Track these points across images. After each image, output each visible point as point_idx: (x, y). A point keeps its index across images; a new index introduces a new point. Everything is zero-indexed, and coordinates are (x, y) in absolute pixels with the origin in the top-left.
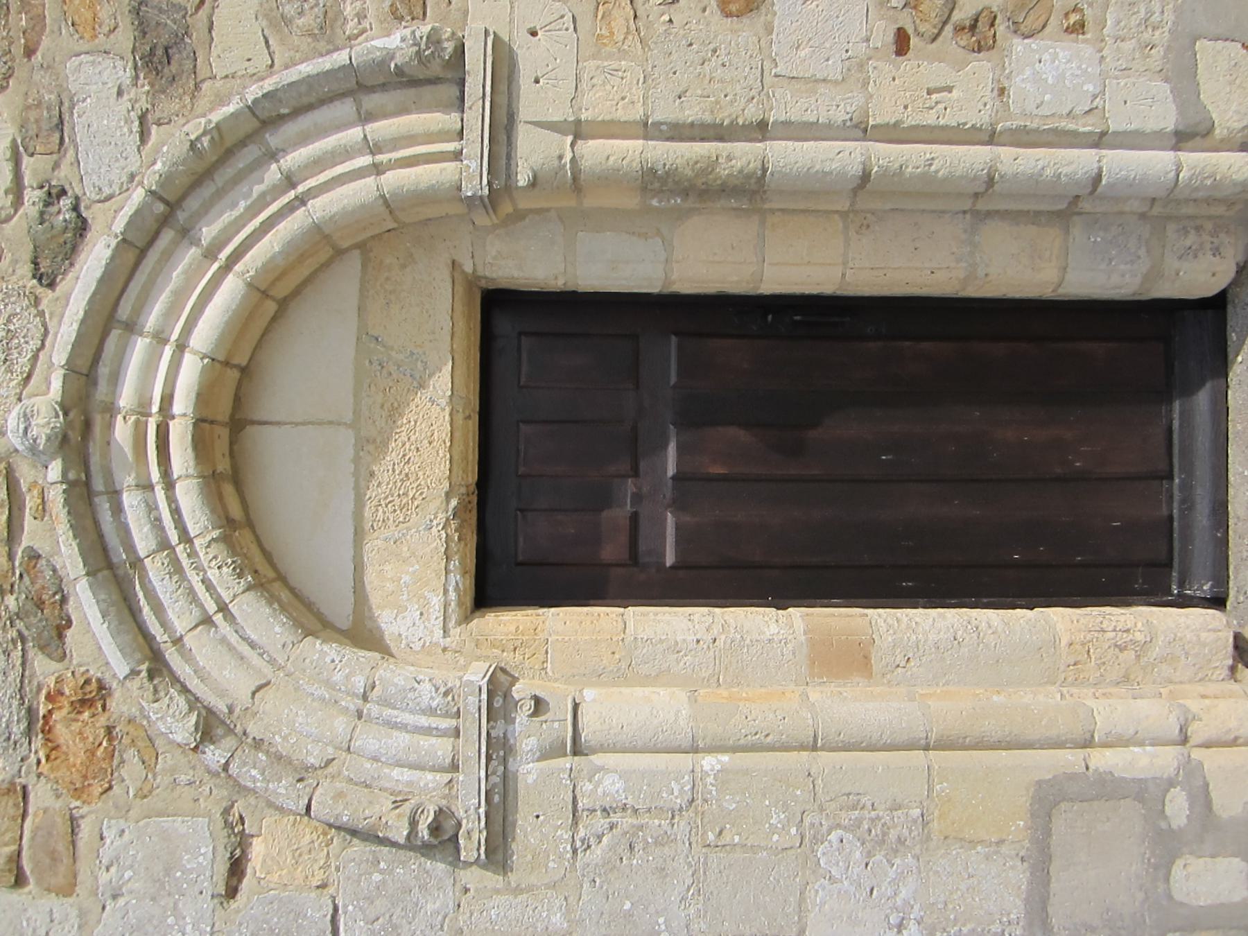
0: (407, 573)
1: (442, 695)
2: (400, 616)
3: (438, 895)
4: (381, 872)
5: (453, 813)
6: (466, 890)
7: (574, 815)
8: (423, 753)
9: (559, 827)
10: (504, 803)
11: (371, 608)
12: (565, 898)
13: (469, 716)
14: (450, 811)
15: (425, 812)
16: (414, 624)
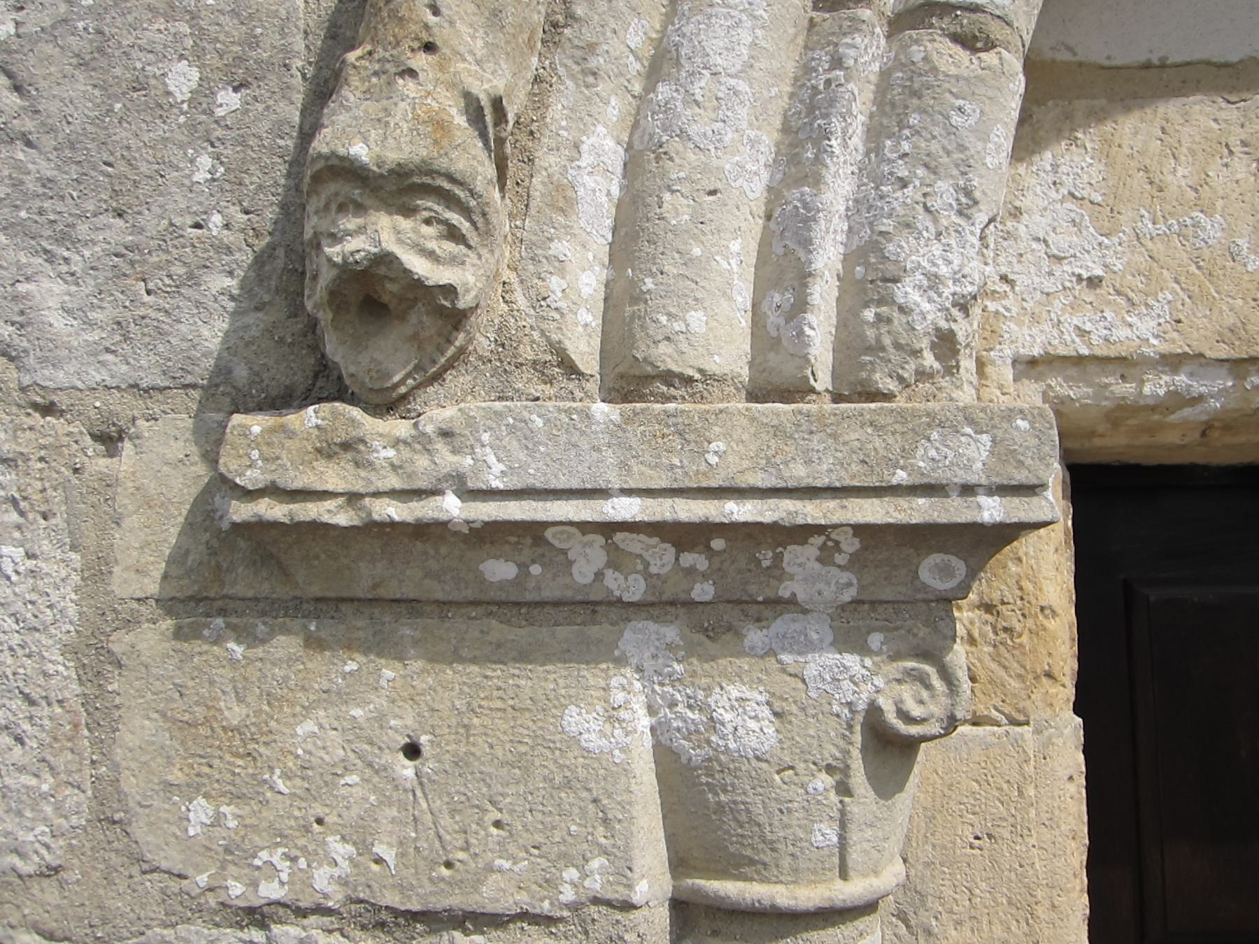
0: (1228, 230)
1: (943, 324)
2: (1085, 213)
3: (91, 324)
4: (202, 96)
5: (437, 377)
6: (110, 440)
7: (414, 916)
8: (697, 251)
9: (364, 847)
10: (475, 603)
11: (1100, 120)
12: (57, 870)
13: (896, 443)
14: (450, 366)
15: (450, 247)
16: (1059, 259)
